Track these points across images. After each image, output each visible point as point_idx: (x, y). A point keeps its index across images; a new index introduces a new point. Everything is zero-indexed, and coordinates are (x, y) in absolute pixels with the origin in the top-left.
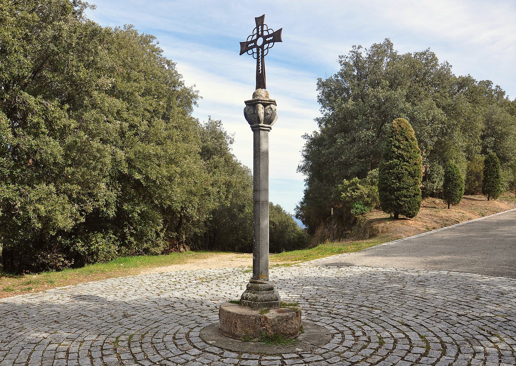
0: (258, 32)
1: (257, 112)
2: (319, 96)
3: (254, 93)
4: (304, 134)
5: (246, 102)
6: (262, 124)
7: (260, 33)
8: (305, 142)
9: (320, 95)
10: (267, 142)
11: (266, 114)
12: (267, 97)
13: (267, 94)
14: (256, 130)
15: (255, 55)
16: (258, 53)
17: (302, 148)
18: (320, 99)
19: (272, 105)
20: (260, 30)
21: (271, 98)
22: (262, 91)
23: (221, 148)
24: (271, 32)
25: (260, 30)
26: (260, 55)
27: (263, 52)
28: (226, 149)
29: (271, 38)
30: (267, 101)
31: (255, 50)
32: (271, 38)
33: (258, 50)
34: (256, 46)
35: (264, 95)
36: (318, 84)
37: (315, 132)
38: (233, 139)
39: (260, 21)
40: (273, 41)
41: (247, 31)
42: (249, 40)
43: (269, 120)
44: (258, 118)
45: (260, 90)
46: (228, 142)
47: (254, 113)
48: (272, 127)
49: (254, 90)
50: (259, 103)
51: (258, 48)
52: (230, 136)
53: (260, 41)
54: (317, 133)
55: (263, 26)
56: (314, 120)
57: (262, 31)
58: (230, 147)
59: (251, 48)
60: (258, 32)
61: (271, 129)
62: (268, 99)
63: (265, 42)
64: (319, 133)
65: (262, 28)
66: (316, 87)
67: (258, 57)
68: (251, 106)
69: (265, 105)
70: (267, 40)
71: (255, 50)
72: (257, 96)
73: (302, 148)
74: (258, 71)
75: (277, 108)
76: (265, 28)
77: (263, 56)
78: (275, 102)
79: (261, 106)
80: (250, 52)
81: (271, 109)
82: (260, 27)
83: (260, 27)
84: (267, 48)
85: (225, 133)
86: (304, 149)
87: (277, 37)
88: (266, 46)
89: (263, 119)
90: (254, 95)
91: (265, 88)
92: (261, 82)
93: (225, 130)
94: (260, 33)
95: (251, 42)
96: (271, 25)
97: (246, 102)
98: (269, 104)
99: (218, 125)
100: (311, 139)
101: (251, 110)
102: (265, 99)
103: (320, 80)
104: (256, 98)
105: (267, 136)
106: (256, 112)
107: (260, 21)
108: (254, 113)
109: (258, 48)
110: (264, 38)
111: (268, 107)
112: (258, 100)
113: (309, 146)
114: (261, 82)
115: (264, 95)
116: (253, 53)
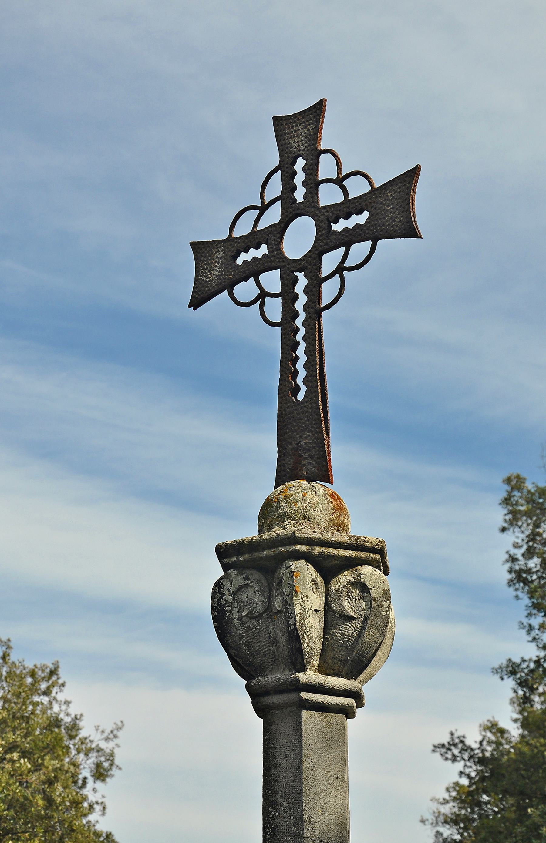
0: (289, 187)
1: (288, 605)
2: (513, 559)
3: (268, 505)
4: (445, 739)
5: (222, 552)
6: (310, 676)
7: (299, 195)
8: (454, 773)
9: (519, 553)
10: (342, 779)
11: (332, 617)
12: (339, 525)
13: (340, 509)
14: (279, 705)
15: (275, 309)
16: (288, 296)
17: (435, 806)
18: (519, 573)
19: (367, 570)
20: (300, 178)
21: (359, 528)
22: (309, 495)
23: (50, 801)
24: (357, 188)
25: (300, 178)
26: (299, 305)
27: (314, 291)
28: (76, 804)
29: (362, 218)
30: (338, 545)
31: (272, 280)
32: (362, 218)
33: (289, 283)
34: (276, 260)
35: (321, 514)
36: (507, 501)
37: (493, 726)
38: (111, 757)
39: (298, 134)
40: (371, 233)
41: (230, 183)
42: (243, 229)
43: (353, 659)
44: (295, 637)
45: (299, 487)
46: (85, 773)
47: (269, 609)
48: (367, 690)
49: (265, 487)
50: (298, 556)
51: (289, 269)
52: (98, 740)
53: (299, 239)
54: (502, 732)
55: (314, 156)
56: (495, 671)
57: (313, 184)
58: (92, 798)
59: (254, 270)
60: (289, 187)
61: (360, 704)
62: (344, 538)
63: (326, 241)
64: (515, 731)
65: (312, 169)
66: (500, 515)
67: (290, 314)
68: (253, 566)
69: (328, 569)
70: (339, 226)
71: (272, 280)
72: (284, 517)
73: (435, 806)
74: (287, 388)
75: (391, 582)
76: (326, 168)
77: (315, 311)
78: (381, 552)
79: (307, 572)
80: (246, 290)
81: (364, 589)
82: (301, 163)
83: (301, 163)
84: (340, 270)
85: (73, 728)
86: (448, 809)
87: (391, 209)
88: (330, 261)
89: (317, 647)
90: (269, 513)
91: (327, 478)
92: (303, 452)
93: (73, 710)
94: (299, 195)
95: (253, 240)
96: (360, 151)
97: (222, 552)
98: (351, 564)
99: (43, 686)
100: (482, 761)
101: (254, 595)
102: (329, 536)
103: (515, 483)
104: (278, 530)
105: (337, 741)
106: (277, 604)
107: (298, 134)
108: (269, 609)
109: (289, 269)
110: (325, 217)
111: (346, 577)
112: (293, 539)
113: (467, 797)
114: (303, 452)
115: (321, 514)
116: (263, 295)
